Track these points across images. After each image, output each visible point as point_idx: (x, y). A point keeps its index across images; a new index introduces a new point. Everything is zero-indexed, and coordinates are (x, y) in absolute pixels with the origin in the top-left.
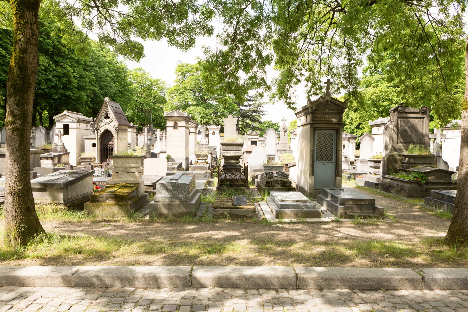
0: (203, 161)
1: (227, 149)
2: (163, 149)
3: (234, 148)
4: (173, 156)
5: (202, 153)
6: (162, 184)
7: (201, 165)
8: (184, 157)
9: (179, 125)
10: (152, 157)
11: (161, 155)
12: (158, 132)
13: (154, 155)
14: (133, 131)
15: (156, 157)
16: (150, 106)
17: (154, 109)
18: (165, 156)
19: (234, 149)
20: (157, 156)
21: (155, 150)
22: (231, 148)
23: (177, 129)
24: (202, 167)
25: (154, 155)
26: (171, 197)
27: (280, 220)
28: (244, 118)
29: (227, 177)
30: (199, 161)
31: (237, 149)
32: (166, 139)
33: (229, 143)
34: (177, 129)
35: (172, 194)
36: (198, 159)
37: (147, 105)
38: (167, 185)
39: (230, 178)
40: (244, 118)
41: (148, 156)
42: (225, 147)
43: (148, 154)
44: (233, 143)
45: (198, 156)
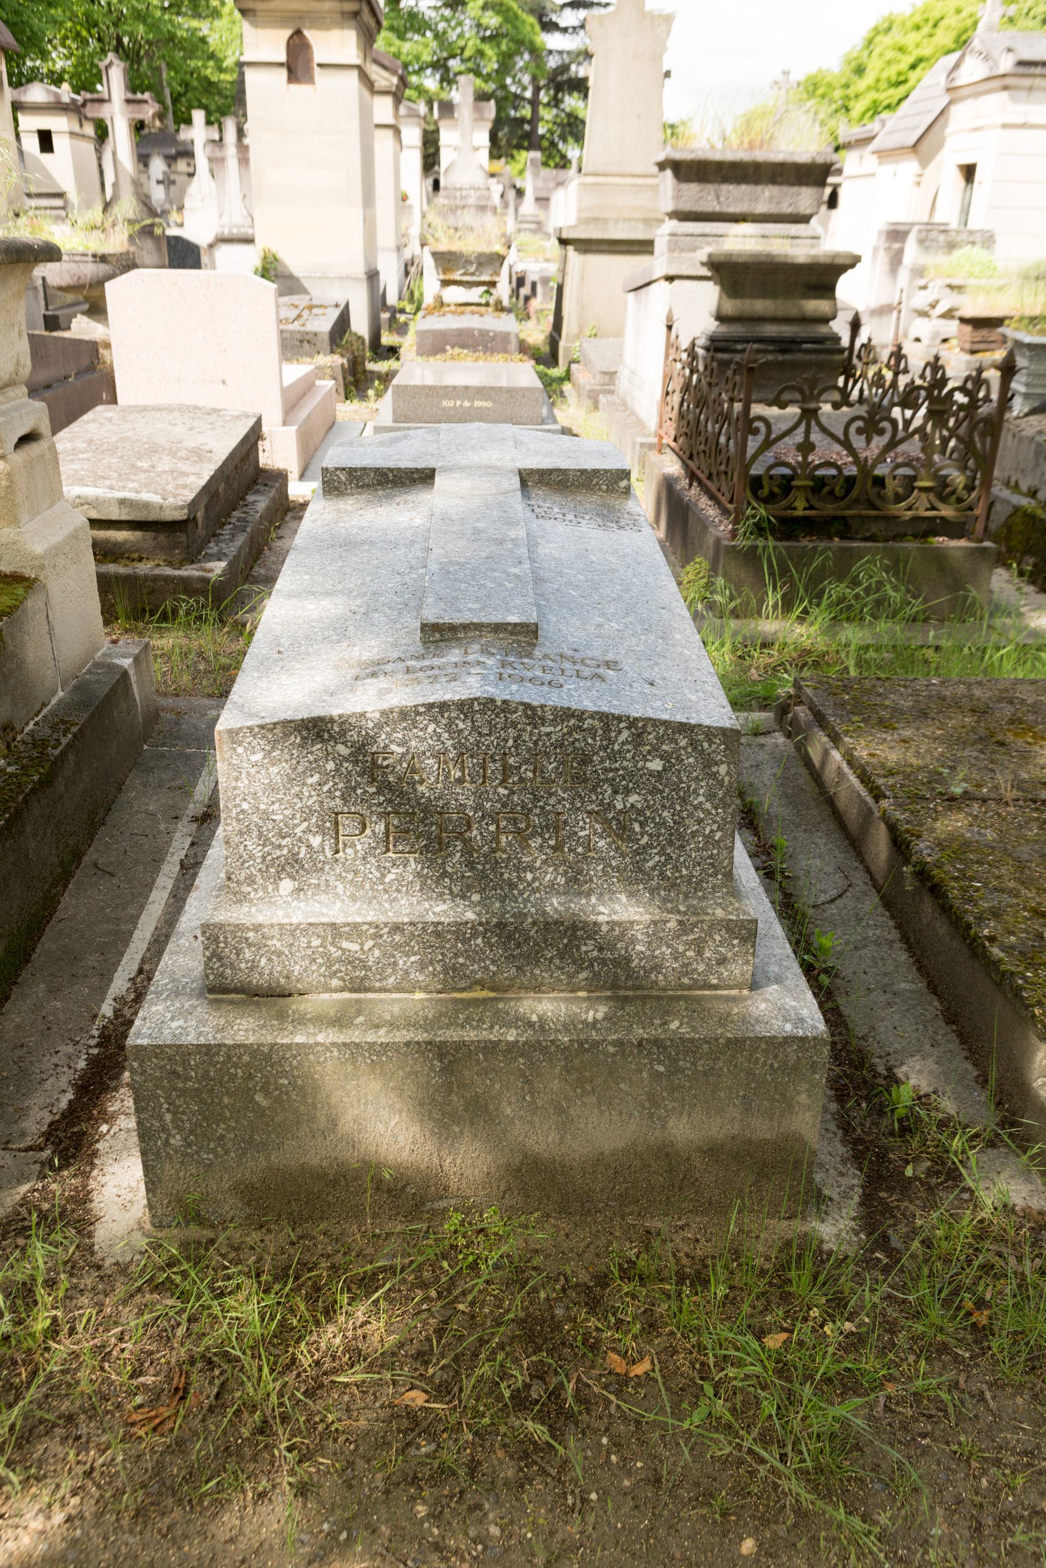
0: (474, 295)
1: (710, 205)
2: (234, 221)
3: (765, 198)
4: (294, 263)
5: (470, 245)
6: (315, 730)
7: (470, 321)
8: (360, 271)
9: (319, 55)
10: (173, 265)
11: (224, 252)
12: (197, 132)
13: (183, 255)
14: (76, 128)
15: (197, 265)
16: (154, 26)
17: (172, 38)
18: (249, 257)
19: (761, 208)
20: (204, 259)
21: (195, 226)
22: (736, 197)
23: (310, 80)
24: (484, 333)
25: (183, 255)
26: (460, 931)
27: (722, 553)
28: (559, 87)
29: (814, 458)
30: (455, 294)
31: (786, 209)
32: (244, 160)
33: (730, 156)
34: (310, 80)
35: (484, 874)
36: (446, 283)
37: (140, 16)
38: (394, 746)
39: (842, 457)
40: (559, 87)
41: (147, 259)
42: (692, 189)
43: (147, 250)
44: (761, 156)
45: (446, 260)
